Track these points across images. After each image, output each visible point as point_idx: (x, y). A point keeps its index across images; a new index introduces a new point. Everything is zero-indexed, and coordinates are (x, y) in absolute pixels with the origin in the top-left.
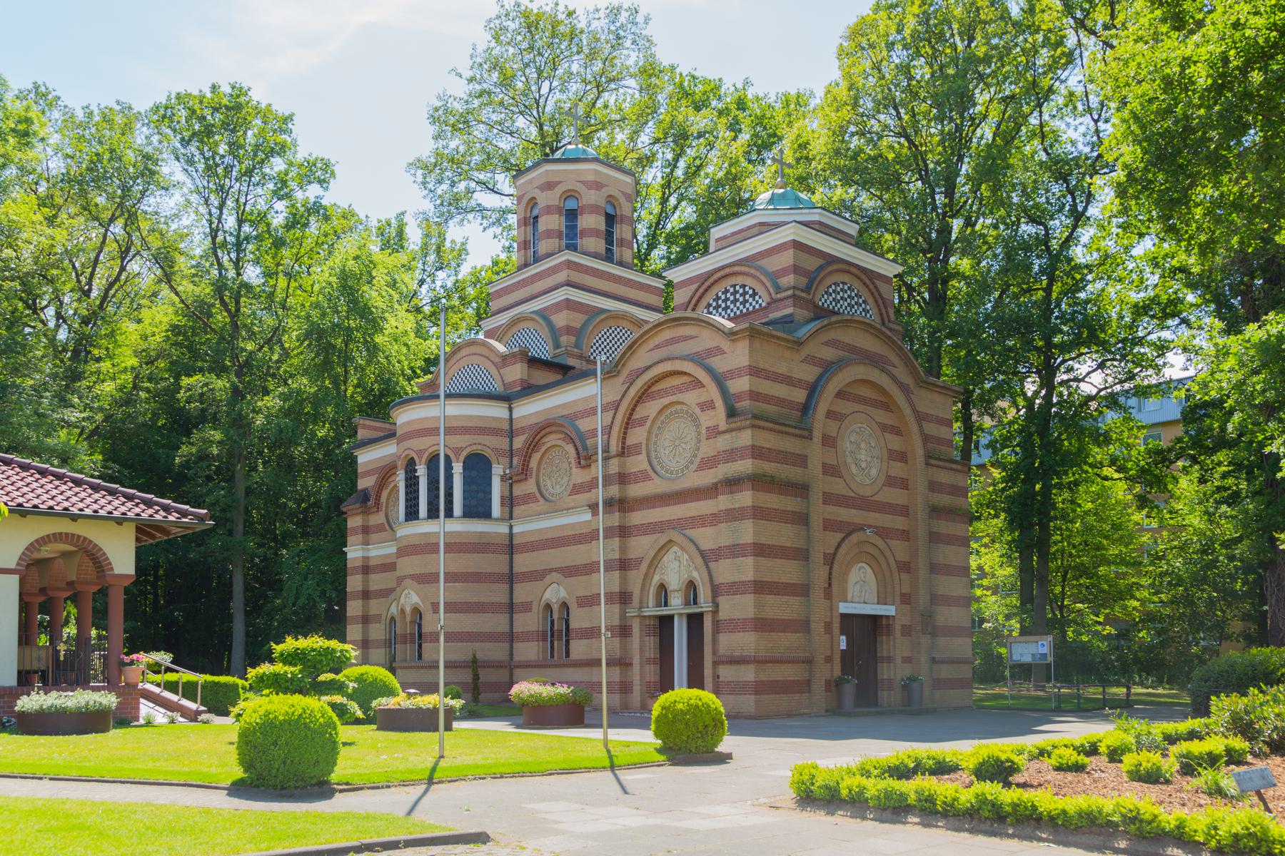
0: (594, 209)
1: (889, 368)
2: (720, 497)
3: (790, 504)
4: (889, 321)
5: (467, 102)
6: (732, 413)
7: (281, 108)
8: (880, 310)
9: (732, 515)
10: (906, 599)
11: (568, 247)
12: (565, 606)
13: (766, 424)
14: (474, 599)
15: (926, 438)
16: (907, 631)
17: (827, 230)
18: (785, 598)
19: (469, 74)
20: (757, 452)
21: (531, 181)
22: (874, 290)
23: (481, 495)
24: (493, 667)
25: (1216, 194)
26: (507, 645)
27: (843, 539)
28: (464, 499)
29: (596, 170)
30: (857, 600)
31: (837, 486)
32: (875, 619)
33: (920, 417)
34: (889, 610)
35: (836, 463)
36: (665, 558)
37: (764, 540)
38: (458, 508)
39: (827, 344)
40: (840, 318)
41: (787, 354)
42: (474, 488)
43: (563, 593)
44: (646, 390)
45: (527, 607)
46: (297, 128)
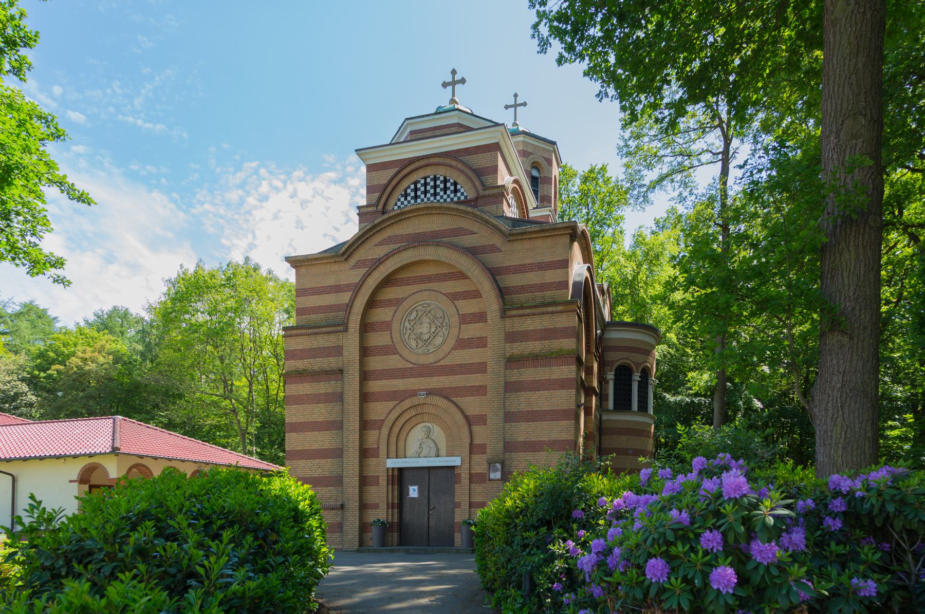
3: (323, 387)
17: (420, 135)
18: (317, 461)
25: (143, 91)
34: (456, 461)
39: (380, 244)
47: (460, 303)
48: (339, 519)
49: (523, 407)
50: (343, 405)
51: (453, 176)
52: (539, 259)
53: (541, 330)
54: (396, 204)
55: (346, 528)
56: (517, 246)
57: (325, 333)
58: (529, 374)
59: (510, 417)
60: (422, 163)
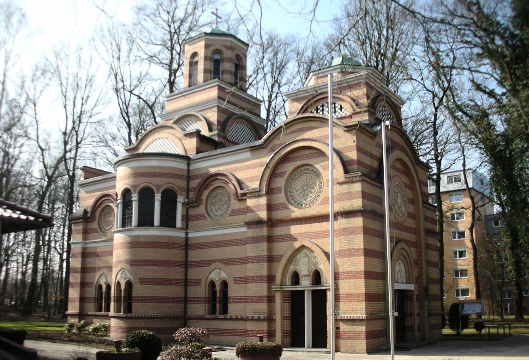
0: (230, 60)
26: (182, 305)
29: (231, 41)
38: (157, 221)
43: (223, 275)
45: (197, 282)
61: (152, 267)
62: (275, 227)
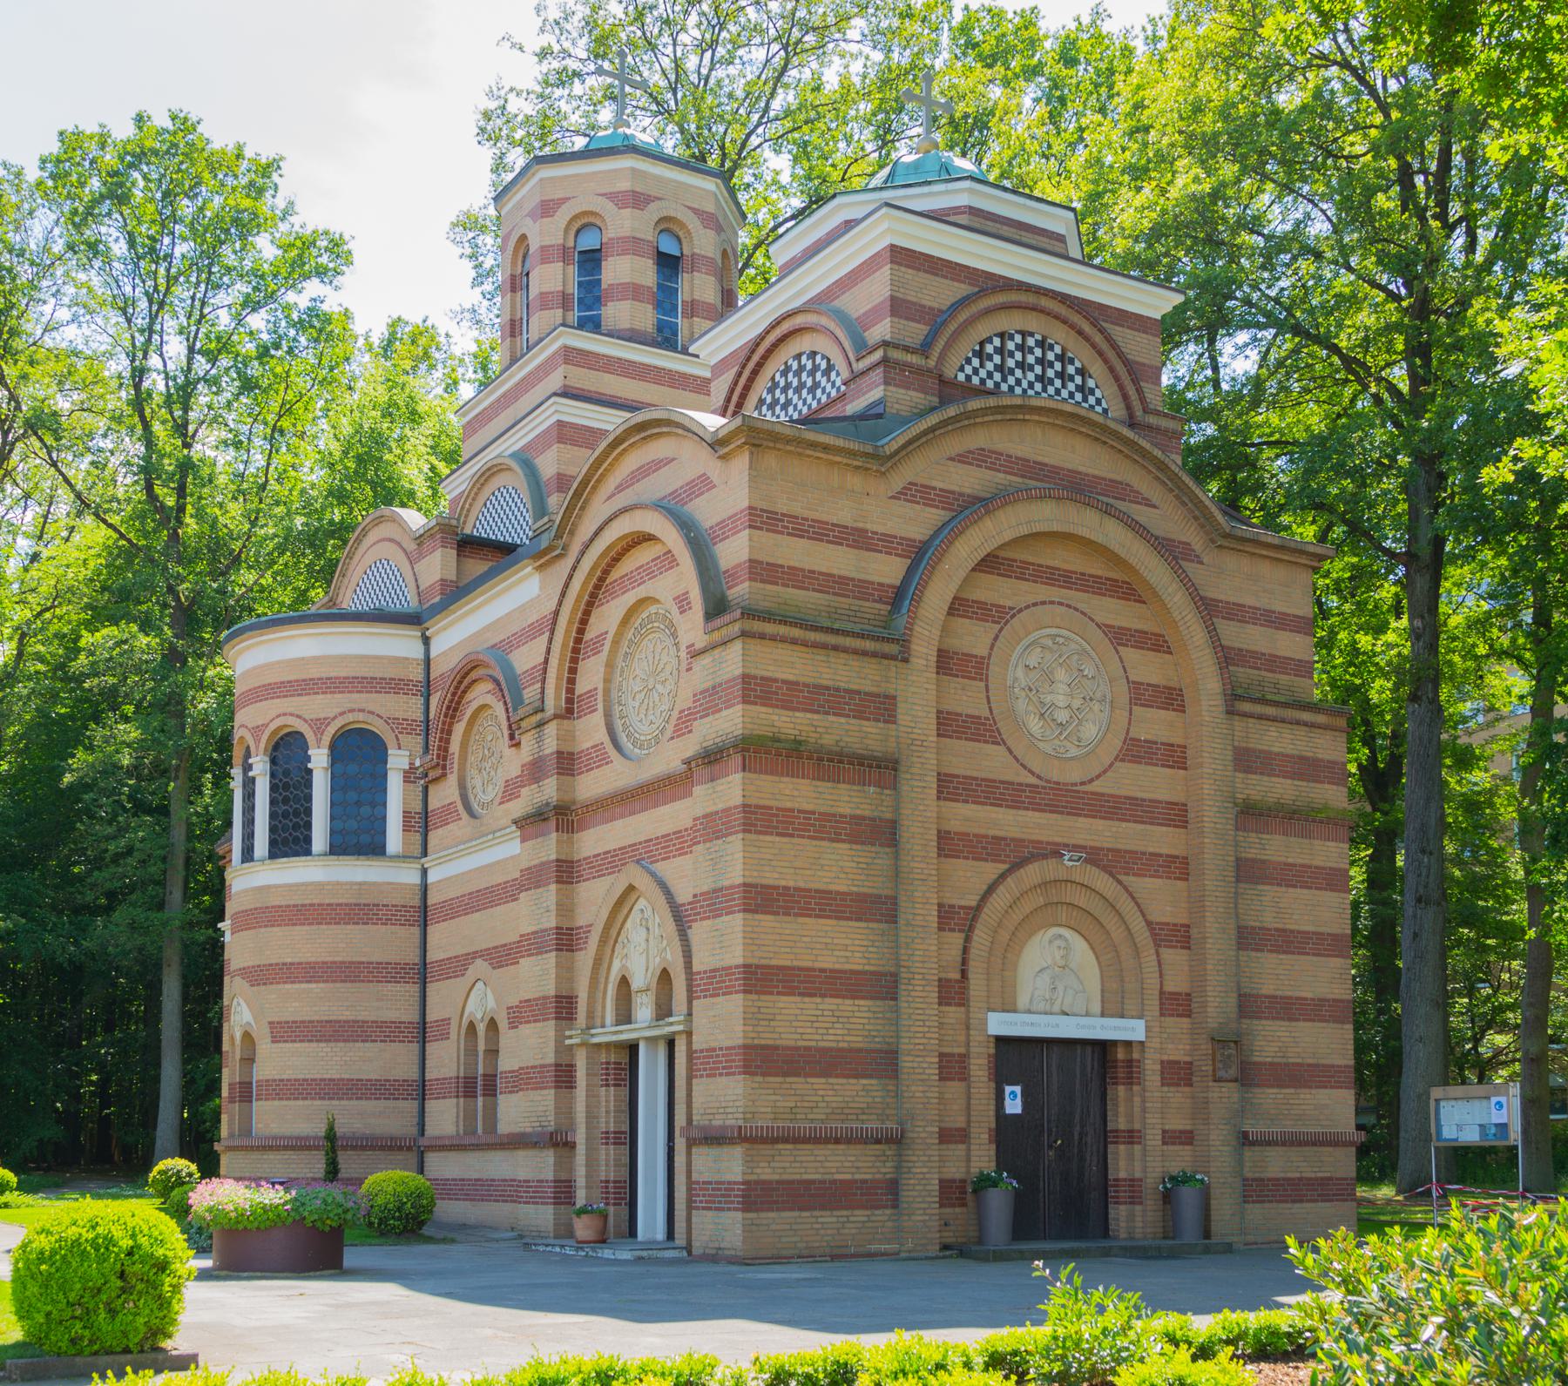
0: (632, 245)
1: (1122, 506)
2: (698, 790)
3: (847, 799)
4: (1146, 410)
5: (541, 96)
6: (716, 608)
7: (259, 148)
8: (1121, 388)
9: (711, 827)
10: (1176, 1004)
11: (582, 325)
12: (492, 1025)
13: (783, 630)
14: (347, 1015)
15: (1227, 657)
16: (1178, 1074)
18: (830, 1003)
19: (536, 43)
20: (754, 689)
21: (519, 205)
22: (1104, 346)
23: (365, 810)
24: (382, 1148)
26: (413, 1106)
27: (1003, 877)
28: (332, 818)
29: (633, 170)
30: (1041, 1007)
31: (989, 762)
32: (1103, 1048)
33: (1209, 609)
34: (1131, 1029)
35: (986, 713)
36: (629, 924)
37: (770, 878)
38: (320, 836)
39: (961, 459)
40: (992, 402)
41: (855, 481)
42: (352, 796)
44: (602, 579)
46: (287, 185)
47: (1130, 654)
48: (886, 1170)
49: (1269, 920)
50: (896, 857)
51: (1082, 355)
52: (1263, 602)
53: (1292, 756)
54: (962, 369)
55: (907, 1195)
56: (1231, 562)
57: (856, 652)
58: (1277, 848)
59: (1248, 938)
60: (1029, 299)
61: (304, 986)
62: (581, 829)
